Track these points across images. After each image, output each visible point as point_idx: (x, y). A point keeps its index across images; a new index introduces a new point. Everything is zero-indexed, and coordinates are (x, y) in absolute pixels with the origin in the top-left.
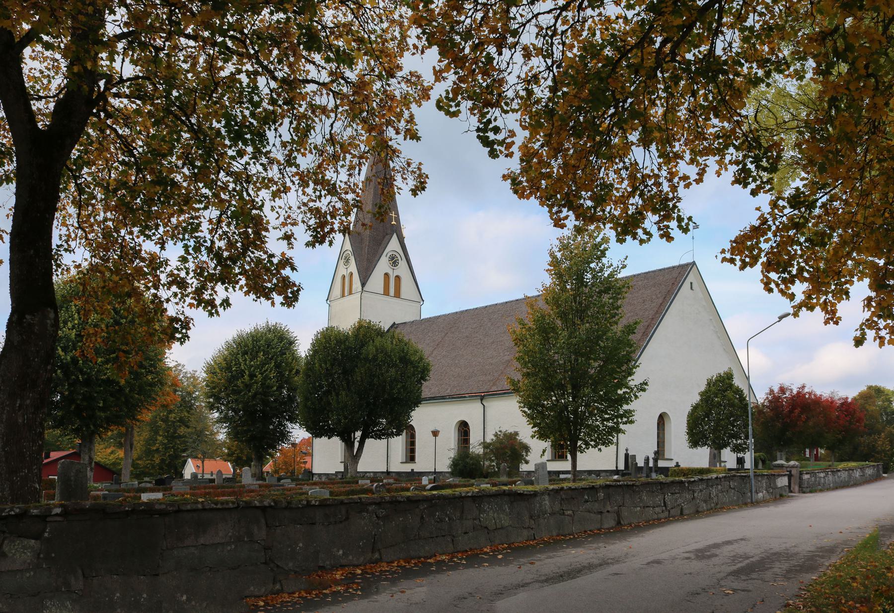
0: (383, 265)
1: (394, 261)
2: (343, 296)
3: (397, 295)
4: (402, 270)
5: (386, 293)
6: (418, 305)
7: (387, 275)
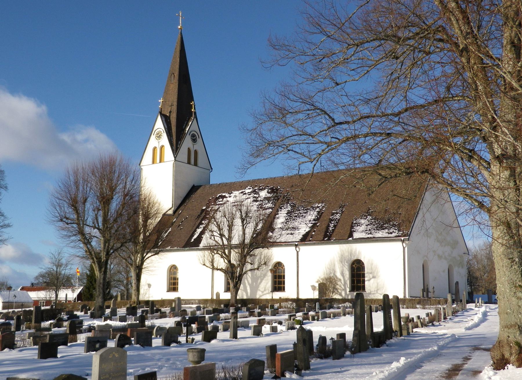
0: (187, 142)
1: (194, 139)
2: (160, 162)
3: (196, 164)
4: (198, 146)
5: (189, 162)
6: (208, 171)
7: (189, 150)
